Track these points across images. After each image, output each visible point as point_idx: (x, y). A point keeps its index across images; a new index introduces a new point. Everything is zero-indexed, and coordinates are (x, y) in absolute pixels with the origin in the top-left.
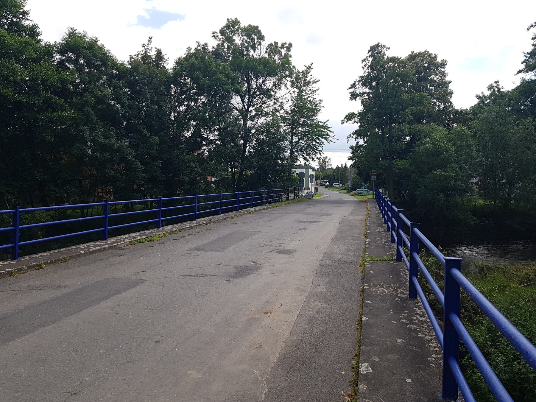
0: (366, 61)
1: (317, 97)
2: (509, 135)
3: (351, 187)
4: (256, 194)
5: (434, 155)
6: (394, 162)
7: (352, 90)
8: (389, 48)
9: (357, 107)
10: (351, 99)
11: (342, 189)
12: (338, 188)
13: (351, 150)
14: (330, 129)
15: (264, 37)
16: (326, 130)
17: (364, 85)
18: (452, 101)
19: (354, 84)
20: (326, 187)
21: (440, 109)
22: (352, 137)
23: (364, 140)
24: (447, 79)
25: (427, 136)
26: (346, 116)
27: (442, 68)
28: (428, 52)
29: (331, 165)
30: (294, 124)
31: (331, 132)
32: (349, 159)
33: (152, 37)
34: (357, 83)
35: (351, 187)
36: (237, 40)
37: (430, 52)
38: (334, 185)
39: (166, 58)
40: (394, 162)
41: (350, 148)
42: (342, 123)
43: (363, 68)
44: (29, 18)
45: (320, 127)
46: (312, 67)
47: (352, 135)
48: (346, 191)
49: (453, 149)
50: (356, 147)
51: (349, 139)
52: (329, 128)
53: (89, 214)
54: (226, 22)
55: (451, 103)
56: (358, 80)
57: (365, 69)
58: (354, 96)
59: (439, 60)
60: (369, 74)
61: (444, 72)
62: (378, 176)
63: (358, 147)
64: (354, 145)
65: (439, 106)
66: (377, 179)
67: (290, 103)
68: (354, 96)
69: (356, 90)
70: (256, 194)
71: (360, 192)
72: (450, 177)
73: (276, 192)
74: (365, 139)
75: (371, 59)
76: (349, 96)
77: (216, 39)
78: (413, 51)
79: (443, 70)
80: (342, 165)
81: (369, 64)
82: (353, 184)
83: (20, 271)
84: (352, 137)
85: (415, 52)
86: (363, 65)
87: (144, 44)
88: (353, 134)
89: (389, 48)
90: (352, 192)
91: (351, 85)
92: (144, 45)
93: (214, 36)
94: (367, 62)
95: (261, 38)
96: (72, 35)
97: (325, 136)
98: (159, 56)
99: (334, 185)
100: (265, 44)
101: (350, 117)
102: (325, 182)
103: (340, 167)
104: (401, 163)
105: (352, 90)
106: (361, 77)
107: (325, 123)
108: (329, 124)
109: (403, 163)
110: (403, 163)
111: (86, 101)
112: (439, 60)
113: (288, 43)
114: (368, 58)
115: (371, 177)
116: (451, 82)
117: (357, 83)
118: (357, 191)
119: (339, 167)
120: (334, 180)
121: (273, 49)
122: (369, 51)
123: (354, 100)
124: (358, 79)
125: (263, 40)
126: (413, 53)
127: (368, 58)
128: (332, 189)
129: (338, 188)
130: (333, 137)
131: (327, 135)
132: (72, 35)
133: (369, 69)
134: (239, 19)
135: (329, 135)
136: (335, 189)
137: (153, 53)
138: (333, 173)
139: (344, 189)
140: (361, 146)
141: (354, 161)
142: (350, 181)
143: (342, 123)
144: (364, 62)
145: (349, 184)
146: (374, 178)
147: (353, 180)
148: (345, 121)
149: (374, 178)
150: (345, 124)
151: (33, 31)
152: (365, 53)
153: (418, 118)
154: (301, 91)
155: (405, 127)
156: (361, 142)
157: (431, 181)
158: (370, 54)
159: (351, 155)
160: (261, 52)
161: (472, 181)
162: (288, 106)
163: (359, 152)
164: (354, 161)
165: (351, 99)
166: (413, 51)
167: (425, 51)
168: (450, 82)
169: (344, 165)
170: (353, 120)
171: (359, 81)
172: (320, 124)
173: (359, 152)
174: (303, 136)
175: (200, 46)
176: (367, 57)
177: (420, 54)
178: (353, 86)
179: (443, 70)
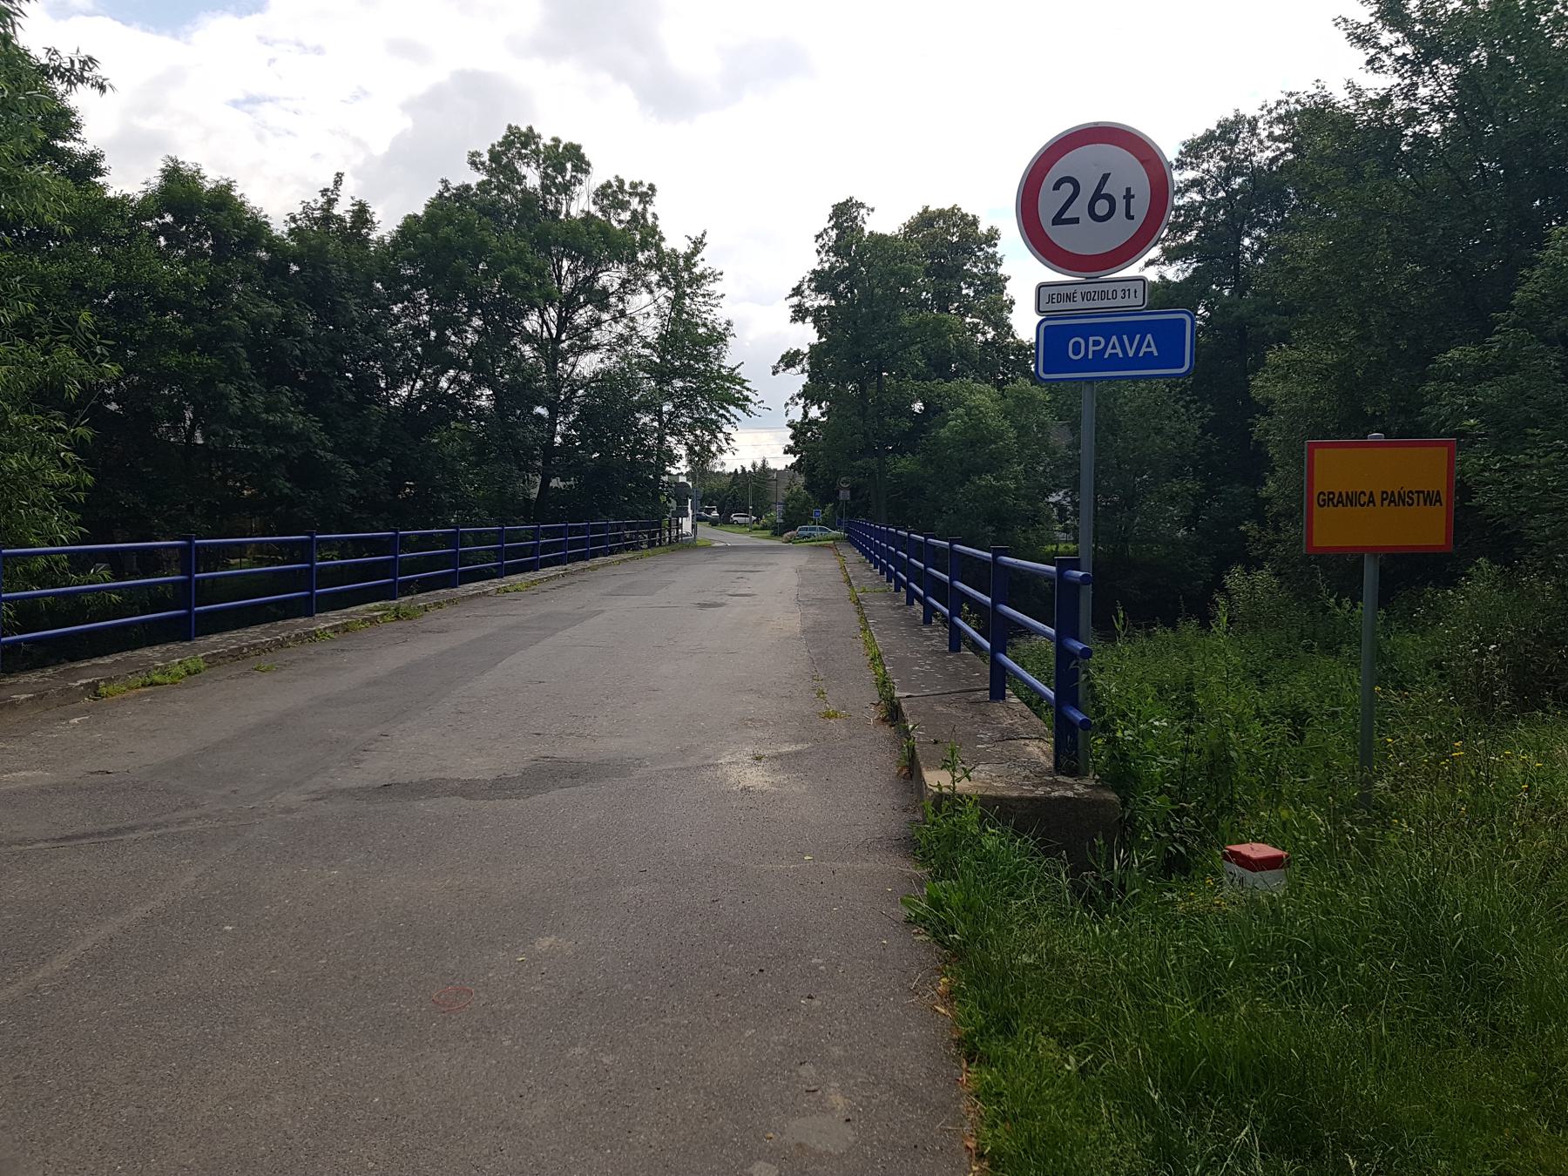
0: (825, 236)
1: (719, 315)
2: (1120, 401)
3: (782, 521)
4: (595, 530)
5: (972, 444)
6: (889, 459)
7: (795, 300)
8: (873, 210)
9: (806, 336)
10: (794, 320)
11: (755, 529)
12: (745, 525)
13: (790, 431)
14: (746, 384)
15: (588, 164)
16: (738, 387)
17: (819, 290)
18: (1011, 322)
19: (799, 287)
20: (714, 523)
21: (987, 340)
22: (797, 404)
23: (820, 407)
24: (1002, 271)
25: (959, 404)
26: (783, 357)
27: (989, 246)
28: (959, 209)
29: (723, 464)
30: (662, 374)
31: (748, 389)
32: (786, 452)
33: (342, 174)
34: (806, 286)
35: (782, 521)
36: (532, 178)
37: (964, 211)
38: (735, 519)
39: (375, 220)
40: (889, 459)
41: (789, 426)
42: (774, 373)
43: (819, 252)
44: (77, 136)
45: (722, 378)
46: (704, 241)
47: (797, 400)
48: (768, 533)
49: (1012, 433)
50: (802, 423)
51: (790, 407)
52: (745, 381)
53: (170, 587)
54: (504, 132)
55: (1010, 327)
56: (807, 279)
57: (823, 255)
58: (800, 313)
59: (983, 228)
60: (832, 268)
61: (994, 255)
62: (854, 490)
63: (807, 424)
64: (798, 418)
65: (984, 334)
66: (852, 498)
67: (654, 321)
68: (800, 313)
69: (805, 300)
70: (595, 530)
71: (806, 533)
72: (1003, 491)
73: (630, 526)
74: (823, 405)
75: (833, 233)
76: (790, 313)
77: (479, 169)
78: (927, 207)
79: (991, 250)
80: (754, 466)
81: (830, 244)
82: (788, 513)
83: (439, 605)
84: (797, 404)
85: (932, 209)
86: (817, 246)
87: (327, 190)
88: (799, 396)
89: (873, 210)
90: (785, 535)
91: (793, 289)
92: (324, 192)
93: (473, 163)
94: (826, 238)
95: (582, 165)
96: (174, 175)
97: (742, 403)
98: (361, 214)
99: (735, 519)
100: (595, 180)
101: (790, 360)
102: (709, 511)
103: (749, 468)
104: (903, 462)
105: (795, 300)
106: (814, 272)
107: (734, 370)
108: (743, 373)
109: (905, 464)
110: (905, 464)
111: (229, 327)
112: (983, 228)
113: (646, 184)
114: (829, 230)
115: (838, 493)
116: (1010, 277)
117: (806, 286)
118: (798, 531)
119: (747, 470)
120: (734, 505)
121: (611, 195)
122: (831, 219)
123: (800, 323)
124: (808, 276)
125: (587, 172)
126: (926, 210)
127: (829, 230)
128: (729, 528)
129: (745, 525)
130: (761, 405)
131: (747, 399)
132: (174, 175)
133: (831, 254)
134: (536, 131)
135: (750, 401)
136: (738, 529)
137: (342, 209)
138: (731, 486)
139: (762, 529)
140: (815, 422)
141: (798, 456)
142: (779, 508)
143: (774, 373)
144: (820, 240)
145: (776, 515)
146: (845, 495)
147: (786, 503)
148: (780, 369)
149: (845, 495)
150: (781, 374)
151: (88, 167)
152: (822, 221)
153: (940, 366)
154: (680, 296)
155: (911, 385)
156: (814, 412)
157: (970, 501)
158: (832, 223)
159: (791, 443)
160: (580, 204)
161: (1051, 500)
162: (650, 328)
163: (809, 434)
164: (798, 456)
165: (794, 320)
166: (927, 207)
167: (953, 208)
168: (1006, 279)
169: (759, 464)
170: (799, 368)
171: (811, 280)
172: (722, 370)
173: (809, 434)
174: (686, 400)
175: (449, 190)
176: (825, 230)
177: (941, 214)
178: (797, 291)
179: (991, 250)
